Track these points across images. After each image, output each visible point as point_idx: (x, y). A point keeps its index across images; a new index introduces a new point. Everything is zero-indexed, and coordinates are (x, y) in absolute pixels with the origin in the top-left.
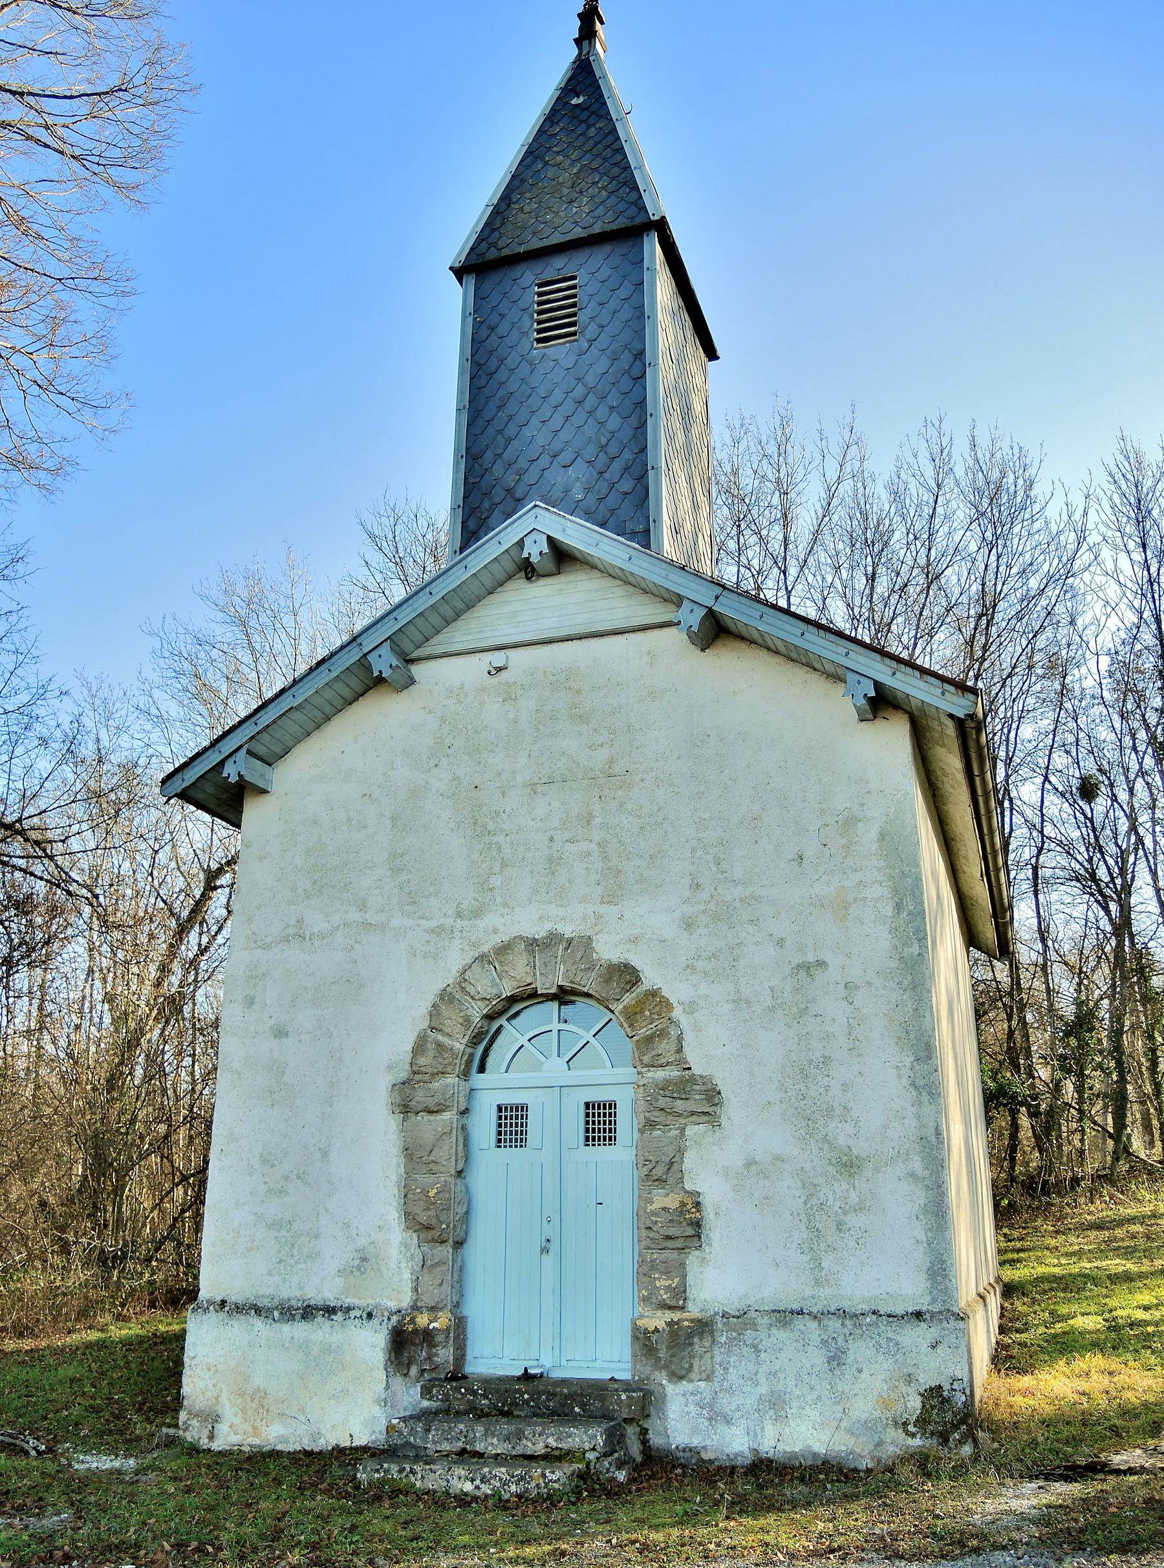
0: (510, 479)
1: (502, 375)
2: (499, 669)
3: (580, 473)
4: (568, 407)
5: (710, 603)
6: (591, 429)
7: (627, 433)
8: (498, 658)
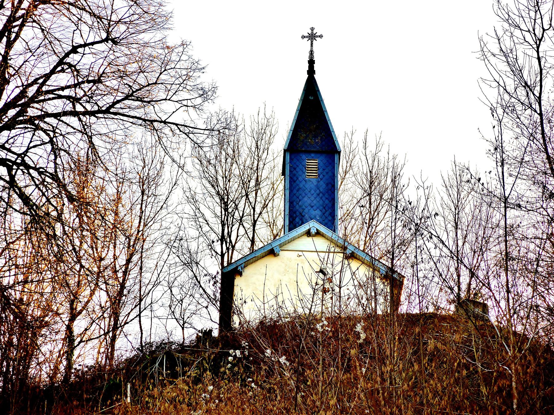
0: (301, 210)
1: (298, 182)
2: (300, 256)
3: (318, 212)
4: (315, 195)
5: (353, 250)
6: (321, 202)
7: (330, 205)
8: (300, 253)
